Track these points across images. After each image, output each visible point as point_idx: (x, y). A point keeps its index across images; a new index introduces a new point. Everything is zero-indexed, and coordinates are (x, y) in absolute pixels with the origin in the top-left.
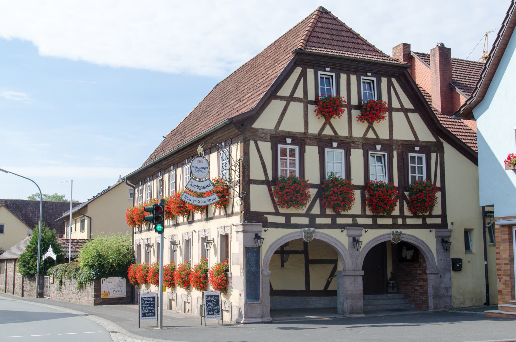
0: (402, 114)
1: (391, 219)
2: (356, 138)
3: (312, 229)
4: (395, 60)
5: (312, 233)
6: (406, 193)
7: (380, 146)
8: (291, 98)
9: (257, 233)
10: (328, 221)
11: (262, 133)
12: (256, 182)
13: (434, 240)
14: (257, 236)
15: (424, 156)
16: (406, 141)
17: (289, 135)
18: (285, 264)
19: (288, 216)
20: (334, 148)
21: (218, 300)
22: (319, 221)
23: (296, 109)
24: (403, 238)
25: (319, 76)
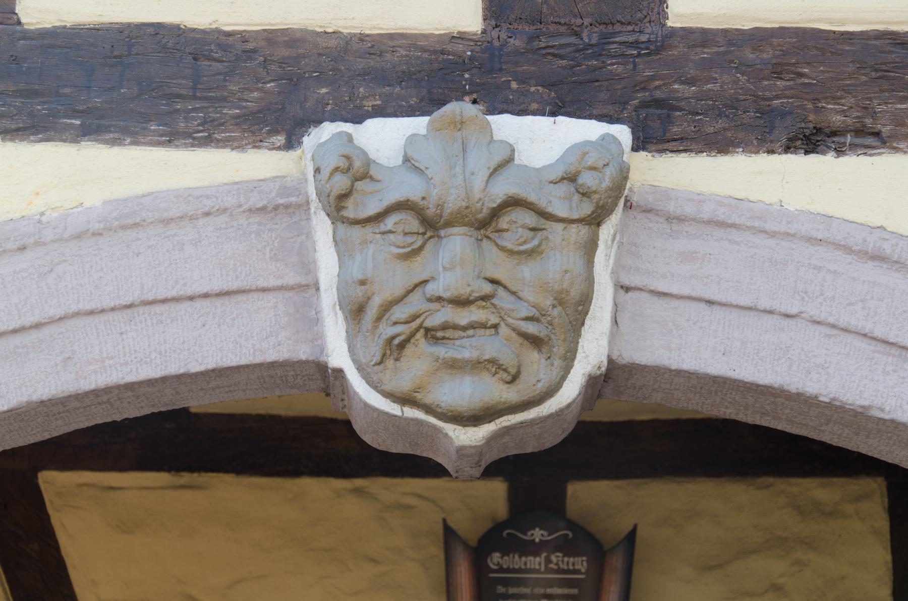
3: (544, 140)
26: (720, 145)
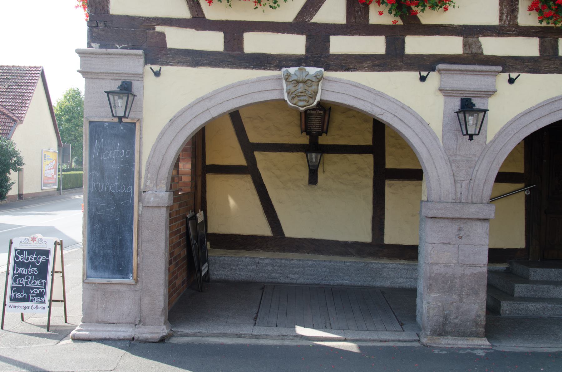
3: (312, 71)
10: (376, 45)
14: (126, 89)
18: (321, 177)
19: (234, 31)
21: (45, 265)
22: (339, 45)
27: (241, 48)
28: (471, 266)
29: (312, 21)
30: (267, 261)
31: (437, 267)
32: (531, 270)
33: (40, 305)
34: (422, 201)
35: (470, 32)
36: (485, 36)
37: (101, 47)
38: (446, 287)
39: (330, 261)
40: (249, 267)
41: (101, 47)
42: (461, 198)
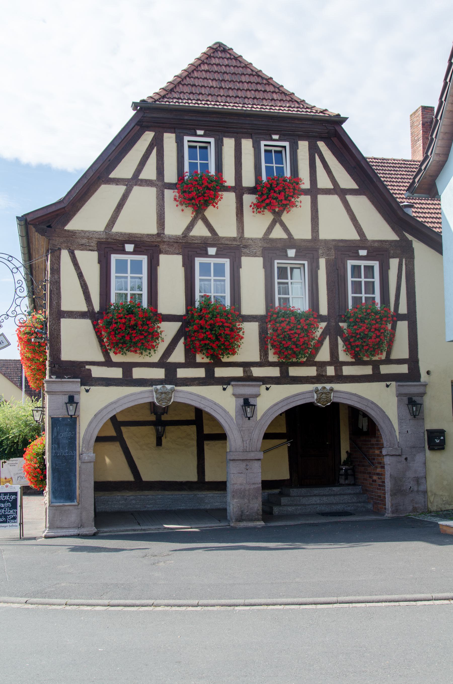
0: (335, 199)
1: (315, 368)
2: (252, 239)
3: (169, 387)
4: (321, 112)
5: (168, 393)
6: (343, 325)
7: (132, 246)
8: (135, 180)
9: (72, 394)
10: (200, 373)
11: (83, 238)
12: (72, 315)
13: (395, 400)
14: (72, 400)
15: (376, 264)
16: (342, 241)
17: (131, 238)
18: (164, 440)
19: (127, 368)
20: (212, 256)
22: (182, 373)
23: (143, 197)
24: (334, 398)
25: (263, 148)
26: (181, 386)
27: (131, 376)
28: (253, 484)
29: (168, 361)
30: (131, 498)
31: (236, 486)
32: (291, 490)
33: (14, 524)
34: (227, 452)
35: (246, 365)
36: (253, 367)
37: (57, 378)
38: (242, 496)
39: (172, 495)
40: (120, 502)
41: (57, 378)
42: (246, 449)
